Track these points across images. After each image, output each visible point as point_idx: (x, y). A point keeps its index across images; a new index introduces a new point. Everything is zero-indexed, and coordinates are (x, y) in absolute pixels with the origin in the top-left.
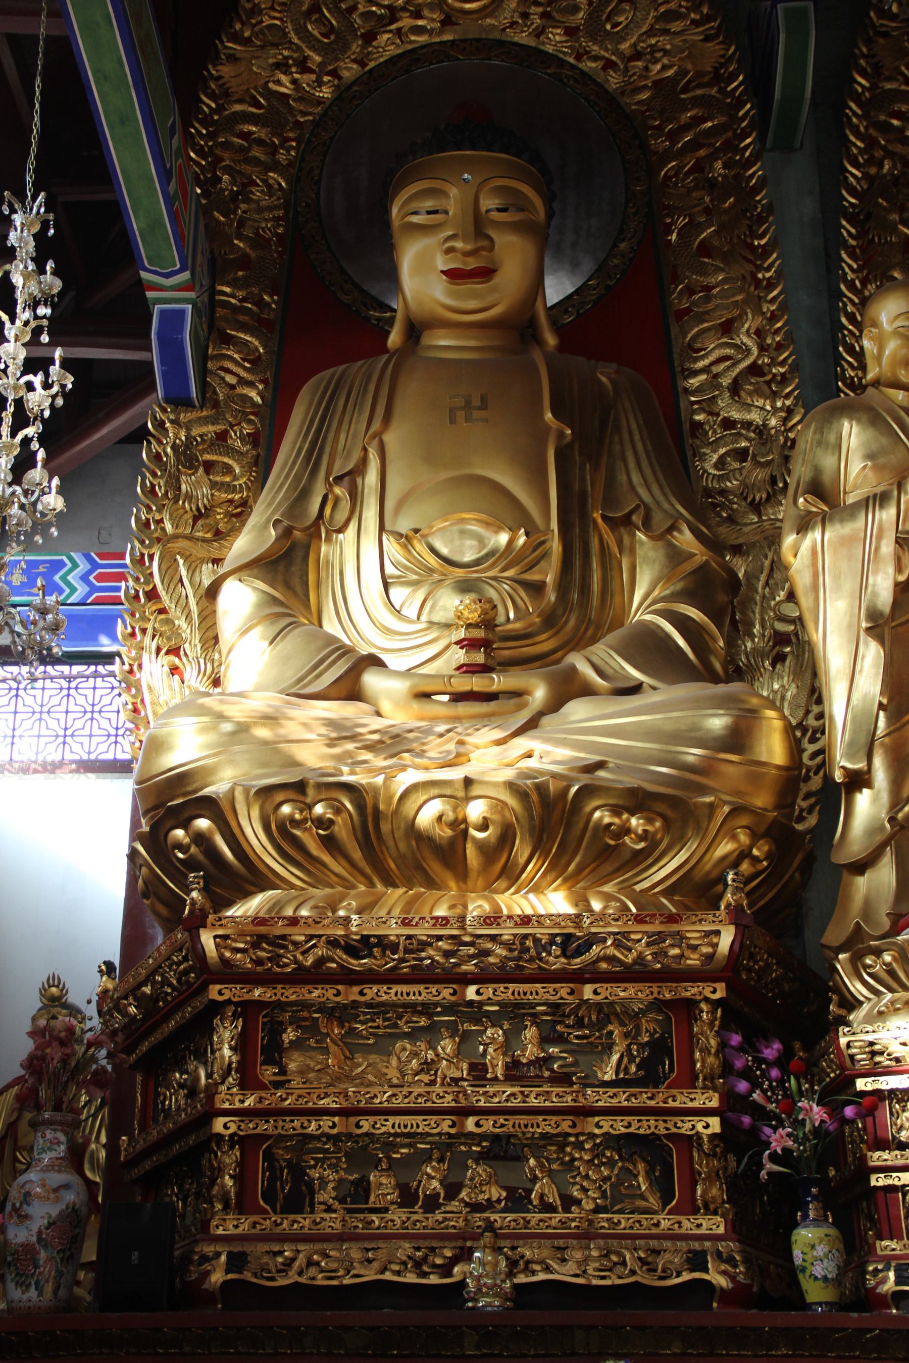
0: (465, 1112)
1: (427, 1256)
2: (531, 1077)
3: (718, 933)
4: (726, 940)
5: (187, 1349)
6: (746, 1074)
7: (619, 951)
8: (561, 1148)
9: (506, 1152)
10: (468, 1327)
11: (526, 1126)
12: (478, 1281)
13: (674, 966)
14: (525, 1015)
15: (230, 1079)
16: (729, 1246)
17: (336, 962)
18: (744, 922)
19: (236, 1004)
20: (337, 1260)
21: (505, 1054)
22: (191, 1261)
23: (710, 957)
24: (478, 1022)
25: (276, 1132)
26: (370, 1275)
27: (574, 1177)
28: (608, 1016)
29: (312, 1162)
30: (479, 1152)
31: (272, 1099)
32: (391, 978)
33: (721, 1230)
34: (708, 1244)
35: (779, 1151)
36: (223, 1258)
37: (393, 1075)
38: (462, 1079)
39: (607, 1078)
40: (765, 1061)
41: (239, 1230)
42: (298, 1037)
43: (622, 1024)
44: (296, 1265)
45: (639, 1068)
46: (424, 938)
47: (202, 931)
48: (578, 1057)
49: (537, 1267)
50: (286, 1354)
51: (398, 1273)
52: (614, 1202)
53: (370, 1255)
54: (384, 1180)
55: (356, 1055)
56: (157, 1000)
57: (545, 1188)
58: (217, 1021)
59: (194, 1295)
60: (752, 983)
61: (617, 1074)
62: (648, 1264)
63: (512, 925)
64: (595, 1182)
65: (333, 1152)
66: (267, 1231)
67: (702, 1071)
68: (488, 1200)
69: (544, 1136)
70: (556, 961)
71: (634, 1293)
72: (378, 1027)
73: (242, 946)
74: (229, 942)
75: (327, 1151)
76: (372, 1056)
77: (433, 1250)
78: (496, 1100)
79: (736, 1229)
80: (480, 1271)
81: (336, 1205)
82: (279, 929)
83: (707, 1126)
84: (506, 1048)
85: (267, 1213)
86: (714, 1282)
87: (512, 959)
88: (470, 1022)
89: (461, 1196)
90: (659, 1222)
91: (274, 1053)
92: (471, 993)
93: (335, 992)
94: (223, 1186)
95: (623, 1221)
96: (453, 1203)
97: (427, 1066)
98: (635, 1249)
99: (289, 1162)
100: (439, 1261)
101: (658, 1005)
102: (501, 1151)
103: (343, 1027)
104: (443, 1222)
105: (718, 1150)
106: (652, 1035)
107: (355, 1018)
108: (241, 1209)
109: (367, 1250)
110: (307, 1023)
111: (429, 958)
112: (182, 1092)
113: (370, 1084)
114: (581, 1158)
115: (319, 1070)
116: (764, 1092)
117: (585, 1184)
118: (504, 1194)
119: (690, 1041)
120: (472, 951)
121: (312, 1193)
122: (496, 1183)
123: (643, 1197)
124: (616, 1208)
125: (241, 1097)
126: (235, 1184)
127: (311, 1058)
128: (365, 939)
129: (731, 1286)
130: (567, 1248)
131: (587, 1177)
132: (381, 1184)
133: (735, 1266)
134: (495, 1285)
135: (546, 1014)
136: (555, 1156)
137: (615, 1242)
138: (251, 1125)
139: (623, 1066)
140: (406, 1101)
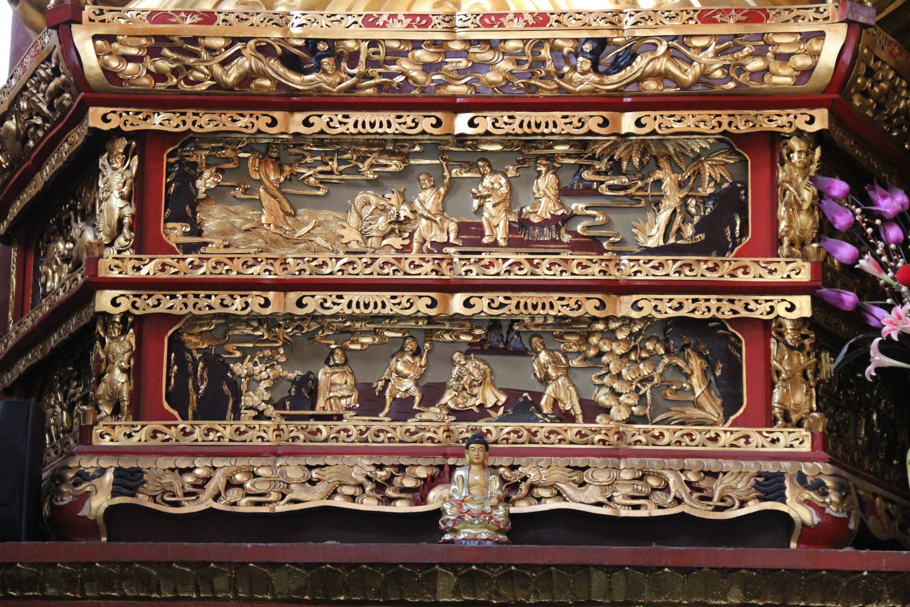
0: (450, 287)
1: (393, 476)
2: (545, 242)
3: (821, 35)
4: (830, 50)
5: (51, 591)
6: (854, 235)
7: (675, 64)
8: (585, 338)
9: (507, 343)
10: (442, 565)
11: (535, 307)
12: (460, 506)
13: (755, 85)
14: (539, 157)
15: (121, 240)
16: (820, 469)
17: (271, 78)
18: (861, 19)
19: (130, 136)
20: (269, 480)
21: (508, 211)
22: (63, 480)
23: (806, 73)
24: (472, 166)
25: (184, 311)
26: (313, 499)
27: (600, 377)
28: (656, 158)
29: (238, 354)
30: (470, 344)
31: (180, 267)
32: (347, 102)
33: (806, 447)
34: (786, 465)
35: (895, 337)
36: (109, 477)
37: (351, 235)
38: (448, 244)
39: (651, 243)
40: (880, 215)
41: (134, 440)
42: (218, 185)
43: (676, 169)
44: (211, 487)
45: (698, 229)
46: (396, 45)
47: (74, 27)
48: (611, 216)
49: (542, 492)
50: (190, 598)
51: (353, 498)
52: (656, 410)
53: (314, 474)
54: (337, 378)
55: (300, 211)
56: (26, 139)
57: (561, 391)
58: (103, 161)
59: (68, 524)
60: (869, 113)
61: (666, 237)
62: (701, 490)
63: (521, 25)
64: (630, 383)
65: (267, 341)
66: (173, 442)
67: (787, 233)
68: (481, 406)
69: (561, 320)
70: (583, 80)
71: (680, 527)
72: (331, 173)
73: (134, 52)
74: (115, 45)
75: (259, 339)
76: (324, 212)
77: (401, 468)
78: (493, 271)
79: (831, 444)
80: (469, 504)
81: (270, 411)
82: (188, 27)
83: (792, 308)
84: (510, 202)
85: (173, 418)
86: (793, 514)
87: (520, 75)
88: (461, 167)
89: (443, 401)
90: (718, 435)
91: (184, 206)
92: (461, 124)
93: (269, 121)
94: (112, 383)
95: (666, 434)
96: (432, 409)
97: (399, 225)
98: (682, 471)
99: (206, 354)
100: (409, 483)
101: (731, 142)
102: (499, 340)
103: (282, 172)
104: (416, 433)
105: (807, 342)
106: (717, 185)
107: (300, 160)
108: (138, 412)
109: (310, 468)
110: (231, 165)
111: (403, 73)
112: (66, 267)
113: (320, 249)
114: (611, 351)
115: (246, 230)
116: (877, 258)
117: (615, 386)
118: (503, 399)
119: (773, 192)
120: (463, 63)
121: (237, 394)
122: (493, 383)
123: (697, 405)
124: (658, 419)
125: (137, 264)
126: (129, 380)
127: (236, 213)
128: (311, 44)
129: (817, 520)
130: (587, 467)
131: (619, 376)
132: (332, 384)
133: (825, 494)
134: (483, 512)
135: (568, 156)
136: (575, 348)
137: (655, 462)
138: (151, 302)
139: (675, 227)
140: (368, 271)
